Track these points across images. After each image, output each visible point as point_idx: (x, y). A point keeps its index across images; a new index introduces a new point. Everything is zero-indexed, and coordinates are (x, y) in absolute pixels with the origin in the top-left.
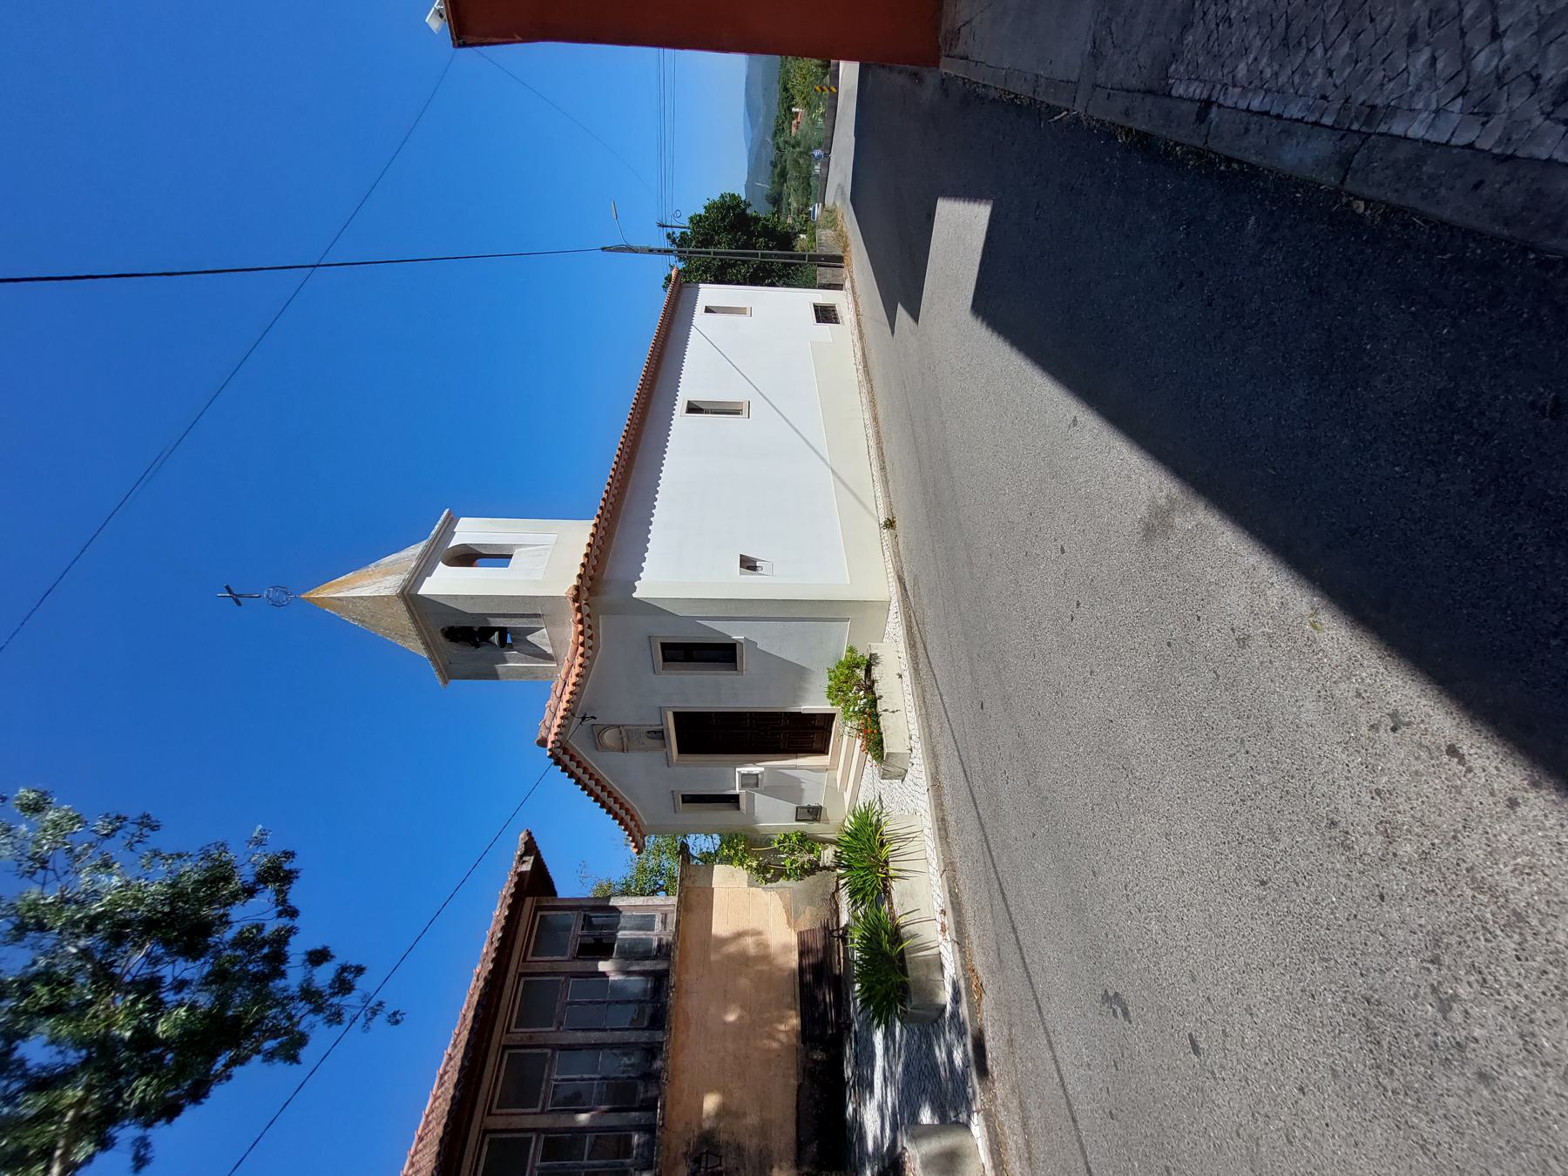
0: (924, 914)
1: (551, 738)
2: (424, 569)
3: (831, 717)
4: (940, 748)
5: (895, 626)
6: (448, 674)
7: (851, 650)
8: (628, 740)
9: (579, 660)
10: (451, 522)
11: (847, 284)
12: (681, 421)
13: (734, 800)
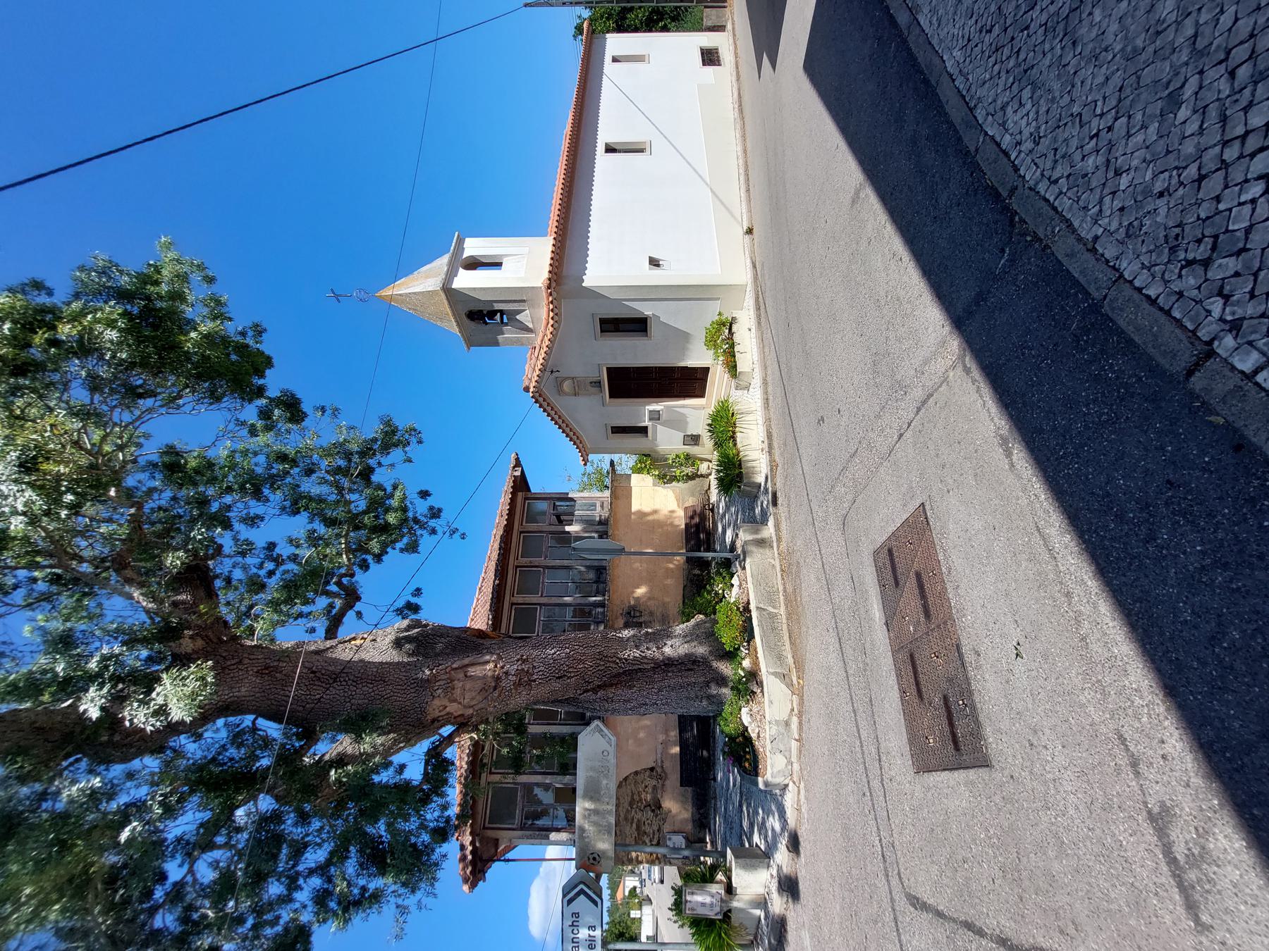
1: (534, 384)
2: (451, 274)
4: (768, 363)
5: (749, 301)
6: (470, 343)
7: (720, 314)
9: (551, 322)
10: (461, 242)
11: (729, 26)
12: (603, 164)
13: (644, 430)
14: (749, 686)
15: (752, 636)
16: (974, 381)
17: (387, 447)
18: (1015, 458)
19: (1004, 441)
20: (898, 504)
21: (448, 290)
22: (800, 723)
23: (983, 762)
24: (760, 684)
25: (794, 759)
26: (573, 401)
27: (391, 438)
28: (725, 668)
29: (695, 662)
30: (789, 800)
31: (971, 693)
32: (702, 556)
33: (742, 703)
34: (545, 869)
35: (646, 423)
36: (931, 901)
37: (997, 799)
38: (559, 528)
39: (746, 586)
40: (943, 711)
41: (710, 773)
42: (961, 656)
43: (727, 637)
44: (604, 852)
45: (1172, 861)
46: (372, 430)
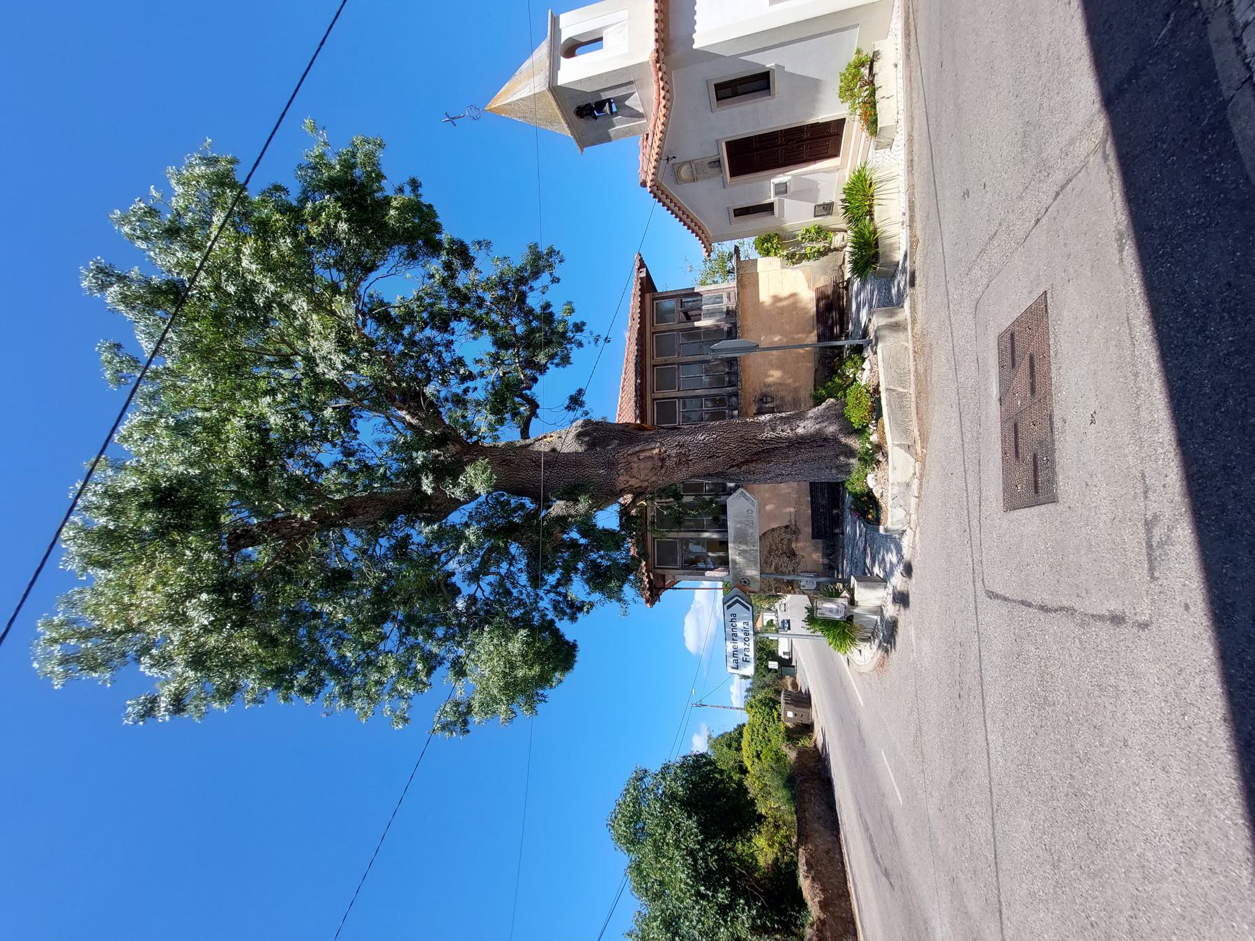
0: (893, 219)
1: (650, 177)
2: (554, 68)
3: (841, 122)
4: (916, 112)
6: (583, 143)
7: (859, 52)
8: (699, 170)
9: (663, 102)
10: (555, 21)
13: (769, 208)
14: (876, 455)
15: (880, 415)
16: (1109, 170)
17: (536, 274)
18: (1125, 253)
19: (1121, 235)
20: (1025, 292)
21: (556, 91)
22: (921, 484)
23: (1053, 500)
24: (885, 455)
25: (912, 511)
26: (689, 188)
27: (540, 262)
28: (854, 443)
29: (826, 439)
30: (906, 542)
31: (1053, 451)
32: (834, 333)
33: (868, 470)
34: (700, 605)
35: (772, 198)
36: (1002, 593)
37: (1057, 523)
38: (688, 325)
39: (875, 370)
40: (1031, 466)
41: (838, 525)
42: (1052, 423)
43: (856, 417)
44: (752, 578)
45: (1149, 546)
46: (519, 258)
